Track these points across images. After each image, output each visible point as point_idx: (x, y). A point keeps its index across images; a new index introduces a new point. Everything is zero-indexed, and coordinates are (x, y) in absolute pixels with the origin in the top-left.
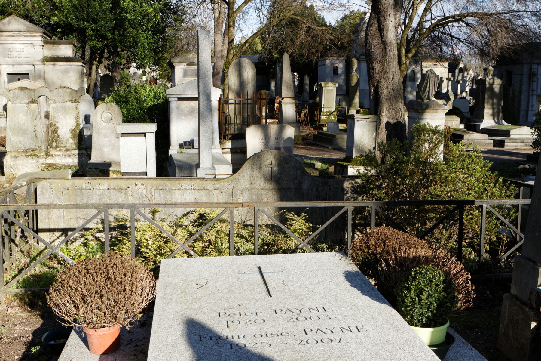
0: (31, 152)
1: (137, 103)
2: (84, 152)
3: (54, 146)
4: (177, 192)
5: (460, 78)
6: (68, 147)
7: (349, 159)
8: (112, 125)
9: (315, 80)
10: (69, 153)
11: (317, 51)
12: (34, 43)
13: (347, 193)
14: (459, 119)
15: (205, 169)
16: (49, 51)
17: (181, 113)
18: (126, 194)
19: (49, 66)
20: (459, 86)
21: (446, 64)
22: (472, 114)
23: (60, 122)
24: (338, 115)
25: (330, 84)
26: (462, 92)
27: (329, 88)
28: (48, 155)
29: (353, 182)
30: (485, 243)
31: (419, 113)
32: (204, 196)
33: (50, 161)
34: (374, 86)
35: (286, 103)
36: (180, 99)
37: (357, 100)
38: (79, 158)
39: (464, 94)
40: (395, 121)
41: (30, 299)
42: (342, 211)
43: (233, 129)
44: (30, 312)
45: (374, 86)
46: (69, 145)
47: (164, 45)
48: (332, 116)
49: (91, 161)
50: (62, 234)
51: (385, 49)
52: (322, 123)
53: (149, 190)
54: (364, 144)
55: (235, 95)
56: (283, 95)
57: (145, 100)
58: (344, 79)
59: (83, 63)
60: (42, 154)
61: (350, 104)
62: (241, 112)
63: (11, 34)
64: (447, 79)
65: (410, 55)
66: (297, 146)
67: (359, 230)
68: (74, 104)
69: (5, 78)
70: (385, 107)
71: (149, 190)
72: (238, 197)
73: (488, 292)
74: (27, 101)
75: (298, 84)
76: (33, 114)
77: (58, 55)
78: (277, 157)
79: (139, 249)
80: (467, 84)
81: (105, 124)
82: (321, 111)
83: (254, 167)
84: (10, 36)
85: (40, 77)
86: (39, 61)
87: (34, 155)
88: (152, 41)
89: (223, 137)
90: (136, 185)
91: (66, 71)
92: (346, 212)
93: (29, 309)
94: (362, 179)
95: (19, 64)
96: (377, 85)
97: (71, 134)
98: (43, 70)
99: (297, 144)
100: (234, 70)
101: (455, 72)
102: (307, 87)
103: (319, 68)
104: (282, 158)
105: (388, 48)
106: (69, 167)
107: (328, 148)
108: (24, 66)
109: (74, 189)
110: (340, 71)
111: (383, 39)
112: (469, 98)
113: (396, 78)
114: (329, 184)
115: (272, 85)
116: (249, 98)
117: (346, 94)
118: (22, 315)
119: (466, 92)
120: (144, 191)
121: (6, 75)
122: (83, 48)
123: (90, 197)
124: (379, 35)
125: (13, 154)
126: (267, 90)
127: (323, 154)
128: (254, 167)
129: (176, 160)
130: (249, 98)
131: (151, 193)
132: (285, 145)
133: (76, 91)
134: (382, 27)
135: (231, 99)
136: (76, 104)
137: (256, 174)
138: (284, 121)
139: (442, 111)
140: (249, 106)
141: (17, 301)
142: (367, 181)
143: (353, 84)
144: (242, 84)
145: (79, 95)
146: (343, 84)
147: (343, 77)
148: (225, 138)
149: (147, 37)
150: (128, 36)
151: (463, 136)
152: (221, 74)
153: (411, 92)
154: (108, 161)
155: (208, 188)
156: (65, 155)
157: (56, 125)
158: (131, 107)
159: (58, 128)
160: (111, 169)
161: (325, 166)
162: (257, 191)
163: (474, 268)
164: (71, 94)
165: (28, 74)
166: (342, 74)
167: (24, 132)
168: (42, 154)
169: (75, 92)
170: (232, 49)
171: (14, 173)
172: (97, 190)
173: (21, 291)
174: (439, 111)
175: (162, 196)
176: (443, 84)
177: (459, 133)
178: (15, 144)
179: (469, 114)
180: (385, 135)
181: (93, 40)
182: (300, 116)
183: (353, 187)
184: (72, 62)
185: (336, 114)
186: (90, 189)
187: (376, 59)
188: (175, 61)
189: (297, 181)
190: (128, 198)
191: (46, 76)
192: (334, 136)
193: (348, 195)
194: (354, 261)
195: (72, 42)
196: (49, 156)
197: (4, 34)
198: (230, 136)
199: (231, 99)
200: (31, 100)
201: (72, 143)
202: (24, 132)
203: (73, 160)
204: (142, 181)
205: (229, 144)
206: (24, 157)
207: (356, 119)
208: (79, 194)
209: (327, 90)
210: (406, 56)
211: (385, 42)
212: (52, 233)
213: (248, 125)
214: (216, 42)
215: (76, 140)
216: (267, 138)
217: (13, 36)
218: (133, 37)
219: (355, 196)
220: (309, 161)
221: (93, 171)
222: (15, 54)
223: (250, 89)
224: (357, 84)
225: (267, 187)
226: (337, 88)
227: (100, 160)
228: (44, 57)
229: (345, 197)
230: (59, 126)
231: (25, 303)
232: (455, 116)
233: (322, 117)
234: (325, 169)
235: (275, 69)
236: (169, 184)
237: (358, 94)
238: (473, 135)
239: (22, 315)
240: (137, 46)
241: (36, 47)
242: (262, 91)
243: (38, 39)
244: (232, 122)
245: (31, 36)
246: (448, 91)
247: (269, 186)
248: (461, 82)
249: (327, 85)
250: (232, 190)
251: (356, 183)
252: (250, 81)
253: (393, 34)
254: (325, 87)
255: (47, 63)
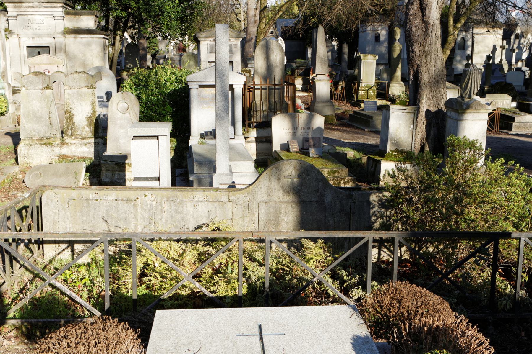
0: (46, 141)
1: (157, 88)
2: (100, 140)
3: (70, 134)
4: (189, 204)
5: (515, 46)
6: (83, 136)
7: (383, 153)
8: (129, 115)
9: (354, 46)
10: (85, 141)
11: (357, 19)
12: (55, 14)
13: (374, 207)
14: (510, 98)
15: (221, 174)
16: (71, 22)
17: (202, 100)
18: (134, 205)
19: (70, 38)
20: (514, 55)
21: (501, 32)
22: (527, 88)
23: (75, 109)
24: (377, 89)
25: (370, 56)
26: (517, 62)
27: (369, 61)
28: (63, 143)
29: (381, 195)
30: (524, 272)
31: (459, 113)
32: (218, 209)
33: (65, 151)
34: (414, 70)
35: (320, 81)
36: (201, 86)
37: (399, 73)
38: (95, 147)
39: (520, 64)
40: (436, 109)
41: (27, 328)
42: (362, 242)
43: (258, 116)
44: (26, 344)
45: (414, 70)
46: (85, 133)
47: (191, 14)
48: (371, 91)
49: (106, 154)
50: (68, 247)
51: (427, 30)
52: (359, 98)
53: (159, 201)
54: (400, 138)
55: (262, 80)
56: (317, 72)
57: (165, 85)
58: (386, 47)
59: (105, 35)
60: (57, 143)
61: (391, 78)
62: (268, 98)
63: (31, 4)
64: (501, 47)
65: (459, 25)
66: (331, 127)
67: (386, 247)
68: (90, 90)
69: (25, 51)
70: (425, 93)
71: (159, 201)
72: (254, 209)
73: (523, 334)
74: (41, 87)
75: (337, 49)
76: (48, 101)
77: (79, 26)
78: (298, 168)
79: (144, 271)
80: (524, 50)
81: (121, 114)
82: (359, 85)
83: (272, 178)
84: (29, 7)
85: (61, 49)
86: (59, 33)
87: (49, 143)
88: (179, 9)
89: (247, 123)
90: (146, 196)
91: (88, 44)
92: (367, 242)
93: (26, 341)
94: (390, 192)
95: (40, 36)
96: (417, 69)
97: (87, 122)
98: (64, 43)
99: (331, 124)
100: (260, 52)
101: (510, 39)
102: (346, 57)
103: (360, 35)
104: (302, 169)
105: (430, 28)
106: (84, 159)
107: (364, 130)
108: (44, 39)
109: (81, 200)
110: (382, 38)
111: (425, 19)
112: (524, 68)
113: (438, 62)
114: (354, 198)
115: (308, 53)
116: (277, 83)
117: (388, 65)
118: (18, 347)
119: (522, 60)
120: (154, 203)
121: (25, 48)
122: (107, 17)
123: (97, 208)
124: (420, 14)
125: (27, 142)
126: (302, 59)
127: (358, 138)
128: (272, 178)
129: (196, 153)
130: (277, 83)
131: (161, 205)
132: (314, 136)
133: (92, 76)
134: (424, 5)
135: (257, 85)
136: (92, 90)
137: (275, 185)
138: (317, 100)
139: (485, 111)
140: (276, 91)
141: (13, 331)
142: (396, 195)
143: (395, 56)
144: (269, 67)
145: (96, 80)
146: (385, 52)
147: (386, 44)
148: (249, 126)
149: (174, 6)
150: (153, 6)
151: (514, 118)
152: (253, 41)
153: (460, 62)
154: (124, 153)
155: (222, 200)
156: (81, 144)
157: (72, 112)
158: (150, 92)
159: (73, 115)
160: (127, 162)
161: (358, 155)
162: (275, 203)
163: (508, 307)
164: (88, 79)
165: (48, 47)
166: (384, 41)
167: (39, 119)
168: (57, 143)
169: (91, 77)
170: (265, 17)
171: (28, 162)
172: (104, 201)
173: (17, 322)
174: (481, 111)
175: (173, 208)
176: (496, 52)
177: (510, 114)
178: (29, 132)
179: (524, 88)
180: (425, 124)
181: (117, 10)
182: (336, 89)
183: (380, 200)
184: (94, 34)
185: (375, 89)
186: (97, 200)
187: (417, 41)
188: (201, 36)
189: (318, 194)
190: (137, 210)
191: (67, 50)
192: (371, 118)
193: (375, 209)
194: (365, 322)
195: (94, 13)
196: (64, 144)
197: (24, 5)
198: (255, 124)
199: (257, 85)
200: (45, 85)
201: (88, 131)
202: (39, 119)
203: (87, 151)
204: (153, 192)
205: (253, 133)
206: (39, 145)
207: (391, 111)
208: (85, 205)
209: (366, 62)
210: (455, 27)
211: (427, 22)
212: (57, 245)
213: (275, 113)
214: (249, 6)
215: (92, 128)
216: (294, 128)
217: (33, 7)
218: (158, 6)
219: (383, 210)
220: (339, 149)
221: (109, 164)
222: (36, 26)
223: (278, 74)
224: (399, 55)
225: (286, 200)
226: (377, 61)
227: (116, 152)
228: (65, 28)
229: (371, 211)
230: (74, 113)
231: (23, 333)
232: (506, 95)
233: (361, 93)
234: (358, 159)
235: (312, 33)
236: (180, 196)
237: (400, 66)
238: (526, 116)
239: (18, 347)
240: (163, 16)
241: (56, 18)
242: (297, 60)
243: (59, 10)
244: (257, 109)
245: (51, 7)
246: (501, 60)
247: (289, 198)
248: (517, 51)
249: (367, 57)
250: (247, 203)
251: (383, 196)
252: (278, 64)
253: (436, 13)
254: (364, 59)
255: (68, 36)
